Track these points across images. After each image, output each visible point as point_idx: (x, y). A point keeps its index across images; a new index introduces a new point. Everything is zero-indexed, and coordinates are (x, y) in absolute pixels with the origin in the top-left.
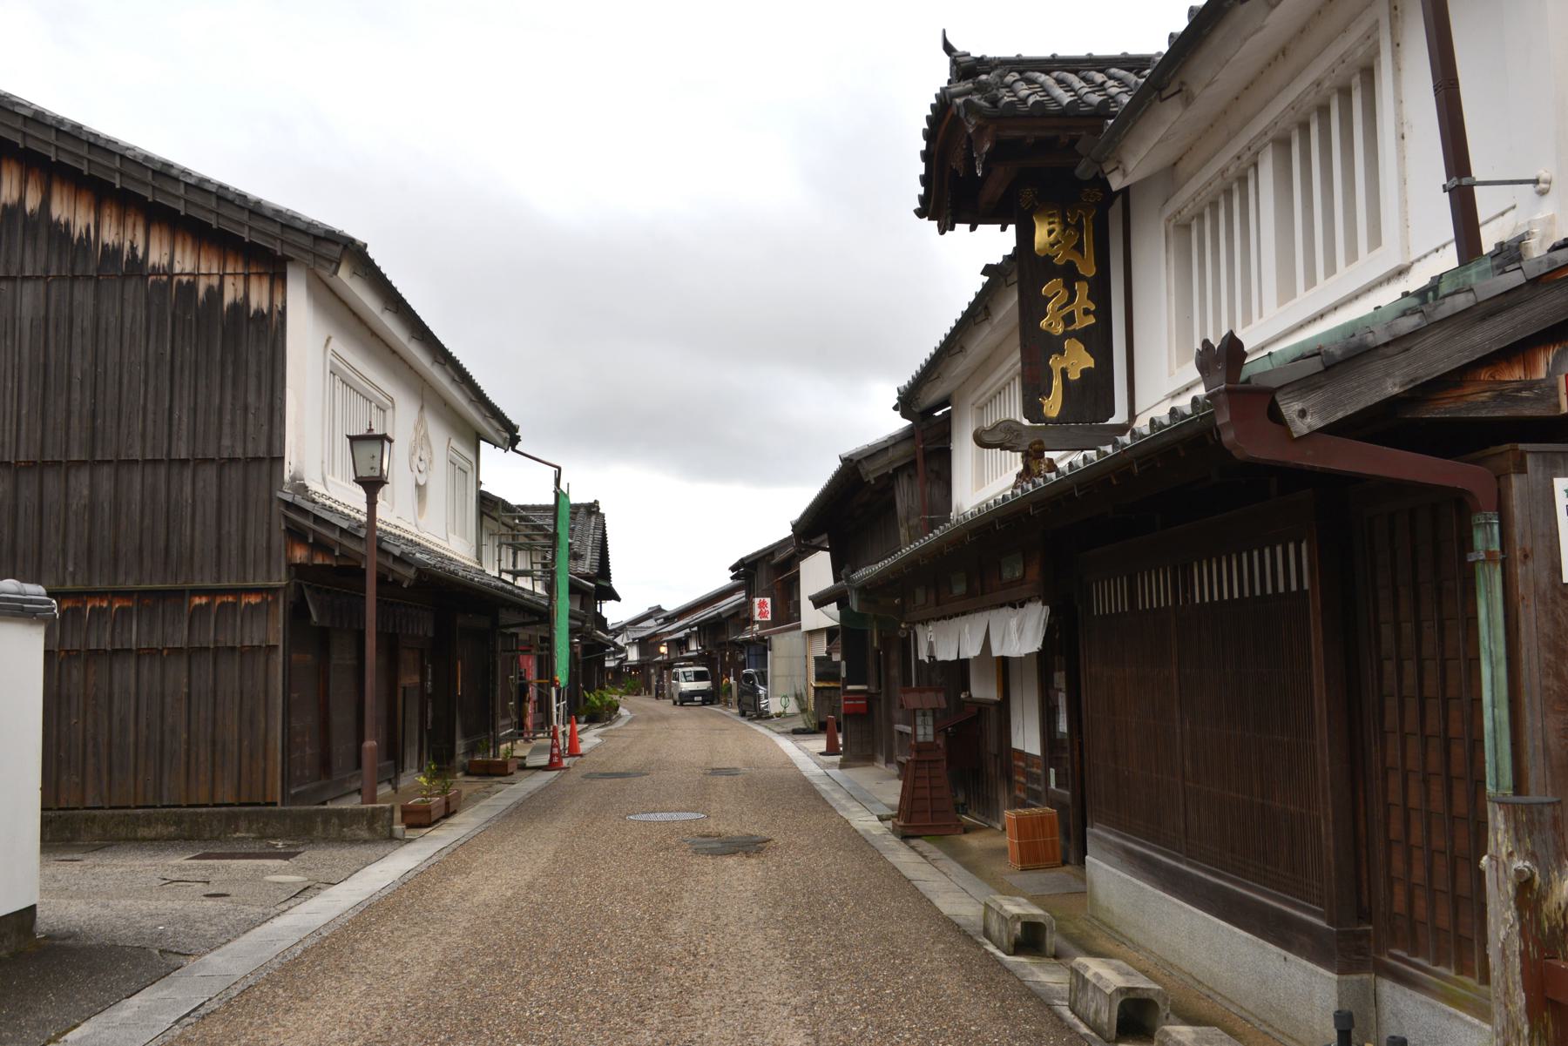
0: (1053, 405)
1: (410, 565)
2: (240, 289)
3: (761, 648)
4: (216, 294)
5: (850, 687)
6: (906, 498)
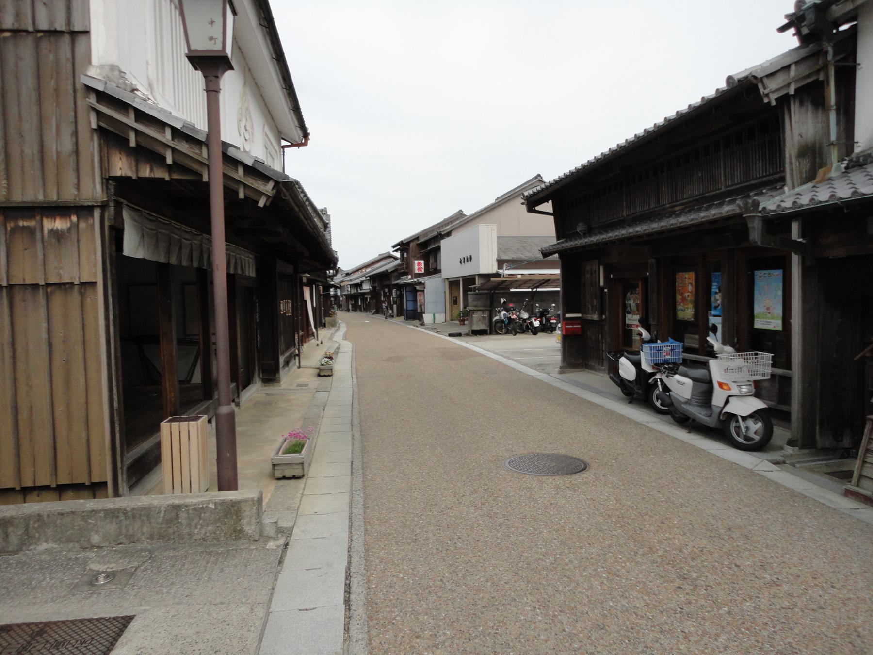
1: (266, 178)
3: (415, 290)
5: (568, 316)
6: (801, 126)
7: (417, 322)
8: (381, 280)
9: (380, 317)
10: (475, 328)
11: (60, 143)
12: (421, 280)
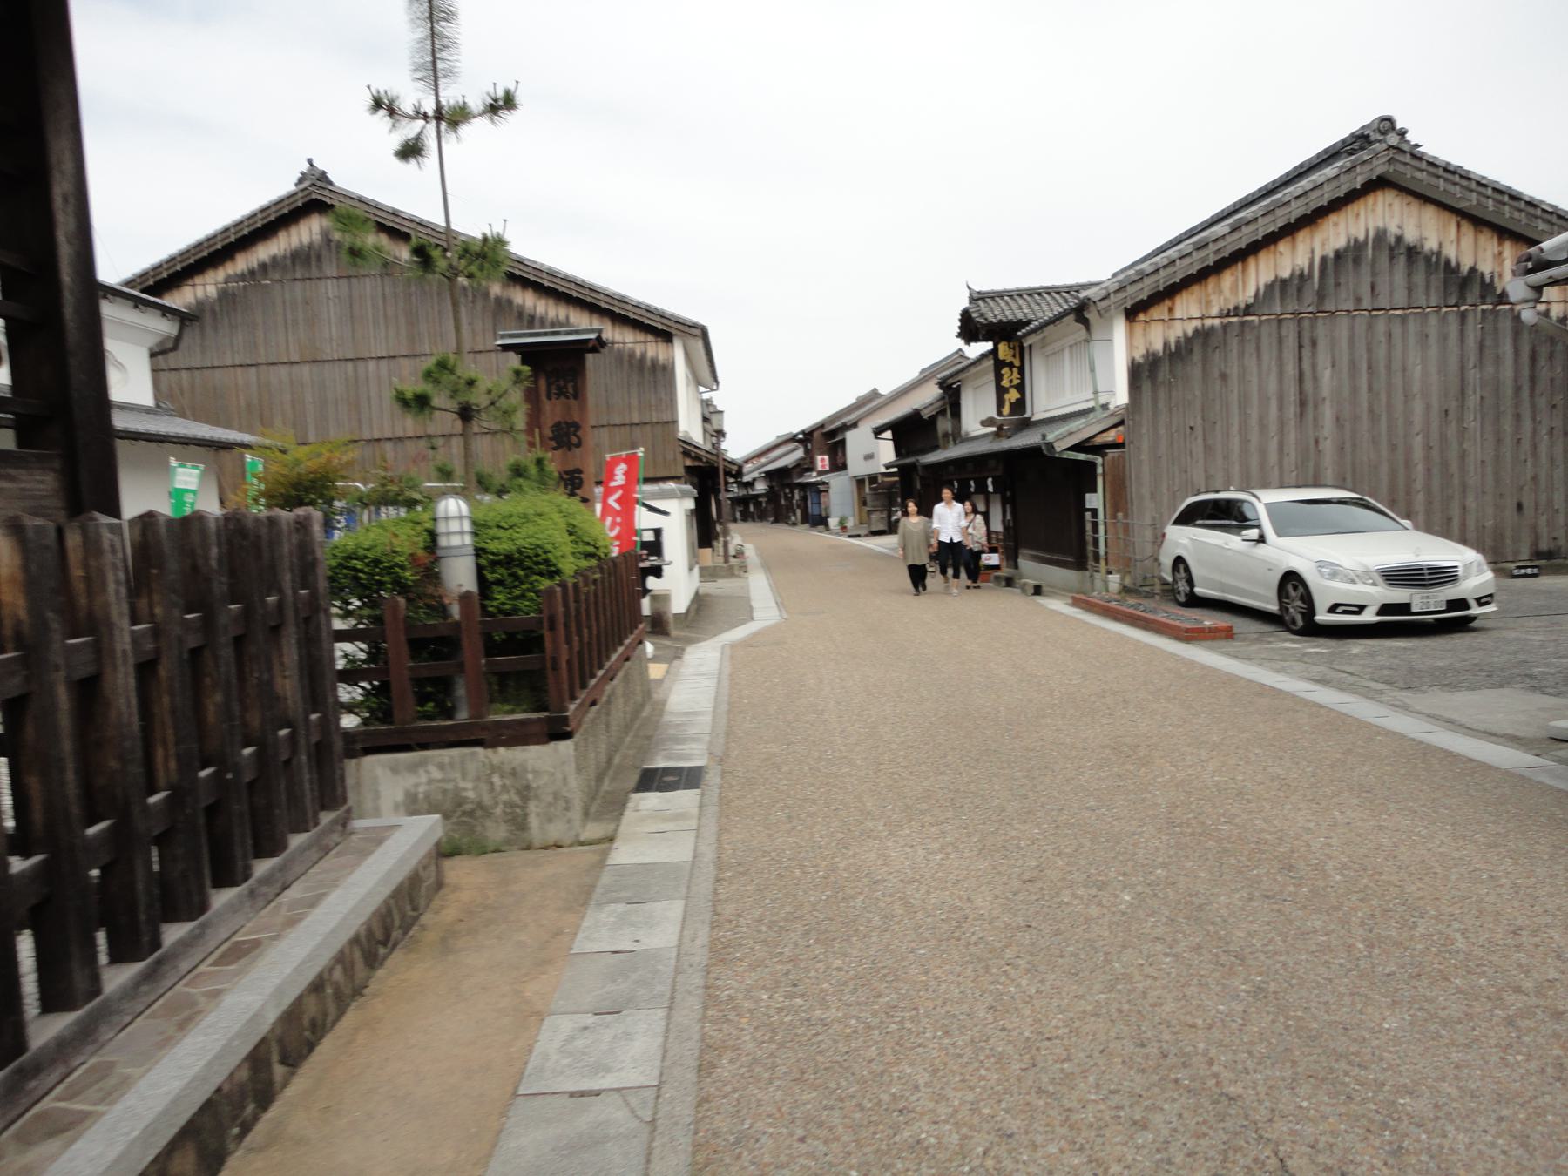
0: (1006, 410)
2: (655, 350)
3: (818, 489)
4: (643, 356)
6: (944, 425)
7: (821, 528)
8: (779, 477)
9: (781, 527)
10: (874, 528)
11: (670, 457)
12: (824, 478)
